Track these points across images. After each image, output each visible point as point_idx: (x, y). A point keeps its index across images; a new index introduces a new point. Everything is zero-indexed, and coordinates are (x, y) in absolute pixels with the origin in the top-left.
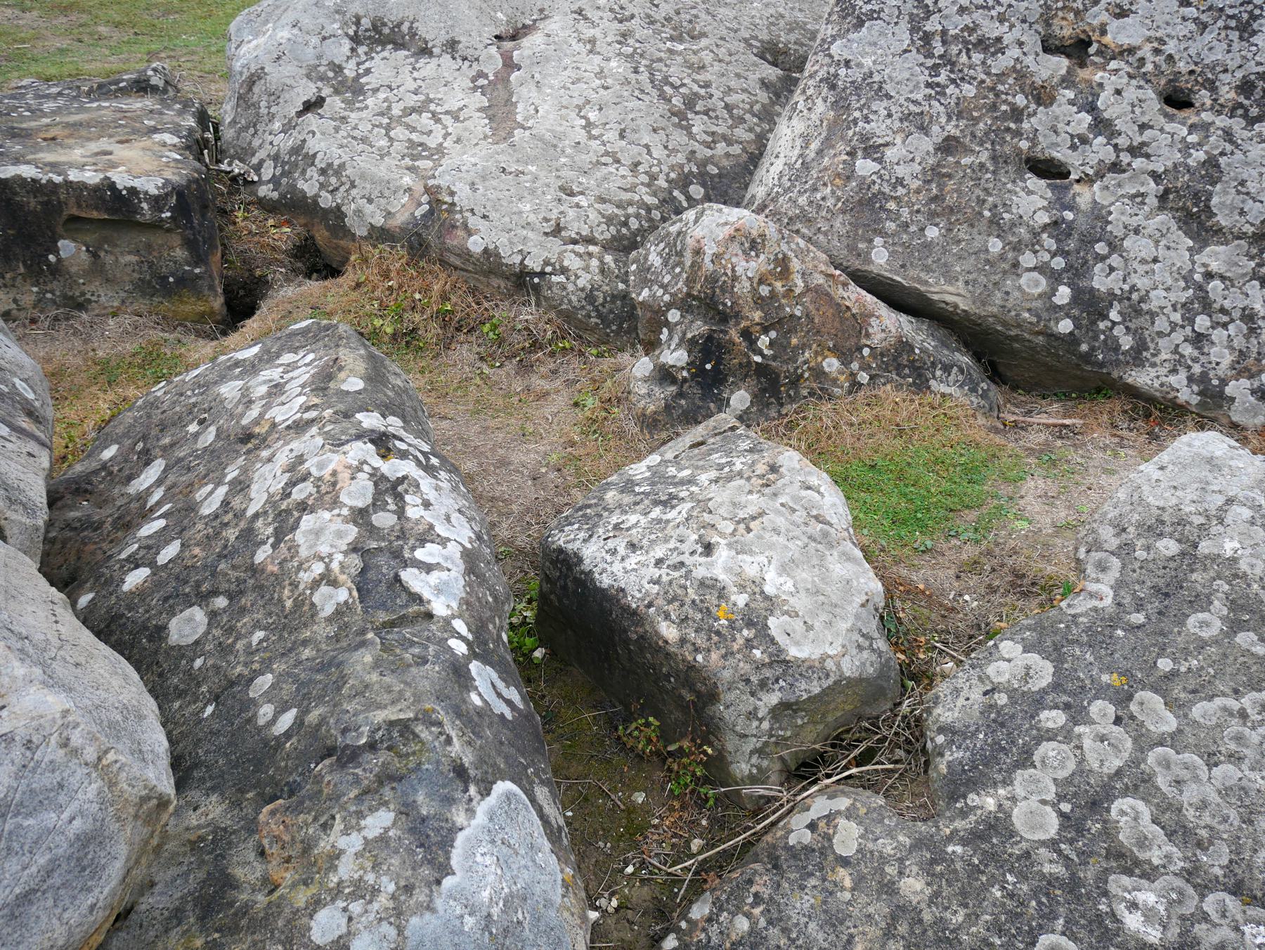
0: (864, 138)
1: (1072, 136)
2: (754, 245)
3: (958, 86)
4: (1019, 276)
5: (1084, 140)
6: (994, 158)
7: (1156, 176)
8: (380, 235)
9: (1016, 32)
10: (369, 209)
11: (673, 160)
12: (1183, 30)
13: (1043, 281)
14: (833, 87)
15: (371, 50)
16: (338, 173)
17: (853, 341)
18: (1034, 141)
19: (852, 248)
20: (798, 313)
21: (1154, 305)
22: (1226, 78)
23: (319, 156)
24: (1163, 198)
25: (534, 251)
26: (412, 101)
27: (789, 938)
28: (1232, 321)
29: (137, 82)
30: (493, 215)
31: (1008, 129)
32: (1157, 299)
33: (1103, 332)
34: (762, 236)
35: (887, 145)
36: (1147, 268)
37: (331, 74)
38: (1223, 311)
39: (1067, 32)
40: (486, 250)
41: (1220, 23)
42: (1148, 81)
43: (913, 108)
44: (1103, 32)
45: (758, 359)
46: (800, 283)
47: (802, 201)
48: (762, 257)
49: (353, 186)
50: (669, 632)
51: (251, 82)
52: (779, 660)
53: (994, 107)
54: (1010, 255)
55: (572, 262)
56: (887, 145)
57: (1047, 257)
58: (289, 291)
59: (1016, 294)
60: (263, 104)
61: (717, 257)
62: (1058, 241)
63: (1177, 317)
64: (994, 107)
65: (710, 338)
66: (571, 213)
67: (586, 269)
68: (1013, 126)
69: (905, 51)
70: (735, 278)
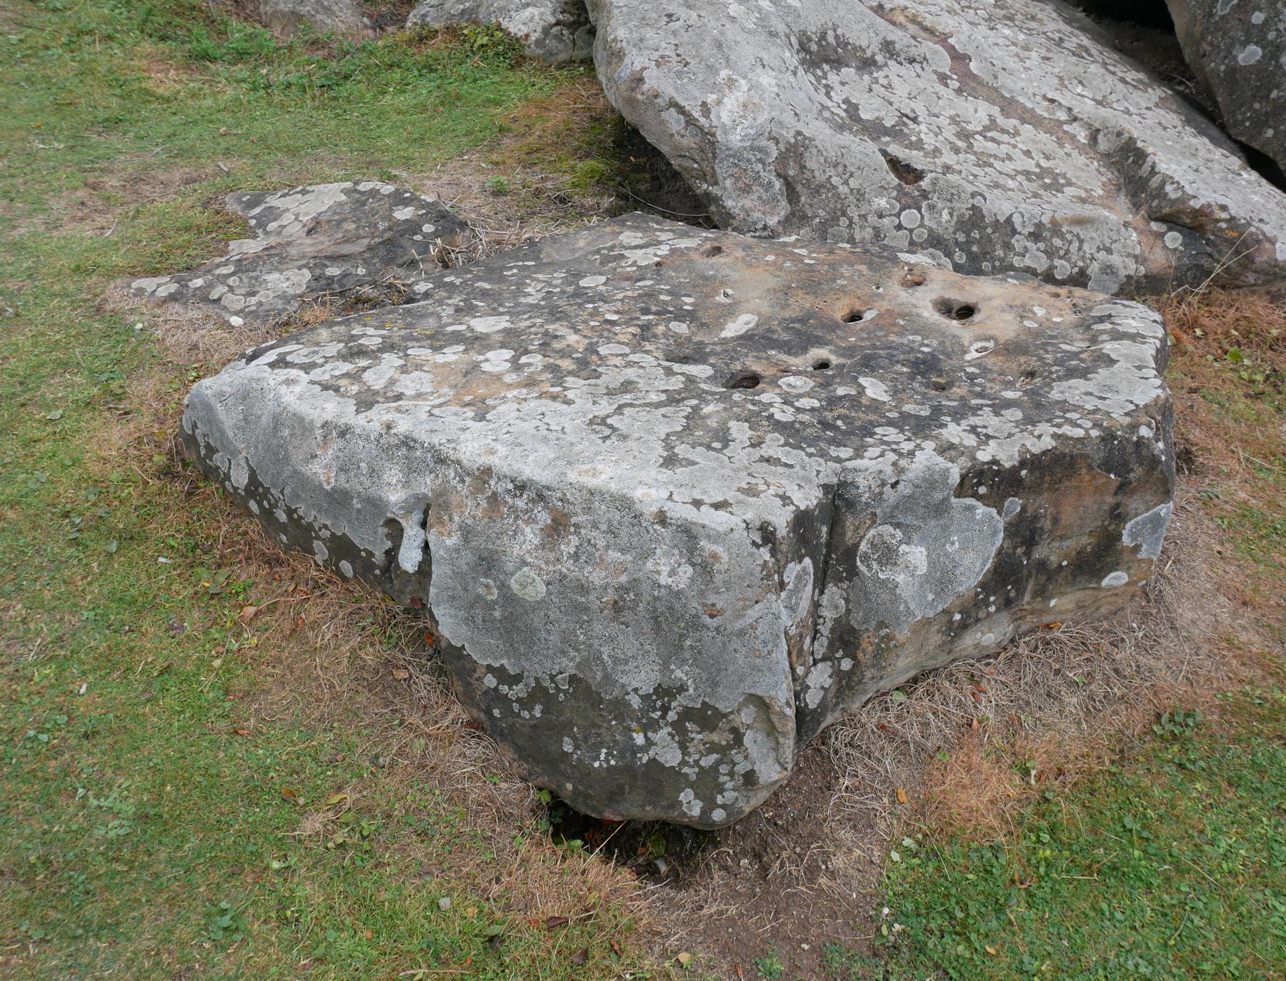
10: (1116, 260)
23: (1017, 219)
60: (835, 180)
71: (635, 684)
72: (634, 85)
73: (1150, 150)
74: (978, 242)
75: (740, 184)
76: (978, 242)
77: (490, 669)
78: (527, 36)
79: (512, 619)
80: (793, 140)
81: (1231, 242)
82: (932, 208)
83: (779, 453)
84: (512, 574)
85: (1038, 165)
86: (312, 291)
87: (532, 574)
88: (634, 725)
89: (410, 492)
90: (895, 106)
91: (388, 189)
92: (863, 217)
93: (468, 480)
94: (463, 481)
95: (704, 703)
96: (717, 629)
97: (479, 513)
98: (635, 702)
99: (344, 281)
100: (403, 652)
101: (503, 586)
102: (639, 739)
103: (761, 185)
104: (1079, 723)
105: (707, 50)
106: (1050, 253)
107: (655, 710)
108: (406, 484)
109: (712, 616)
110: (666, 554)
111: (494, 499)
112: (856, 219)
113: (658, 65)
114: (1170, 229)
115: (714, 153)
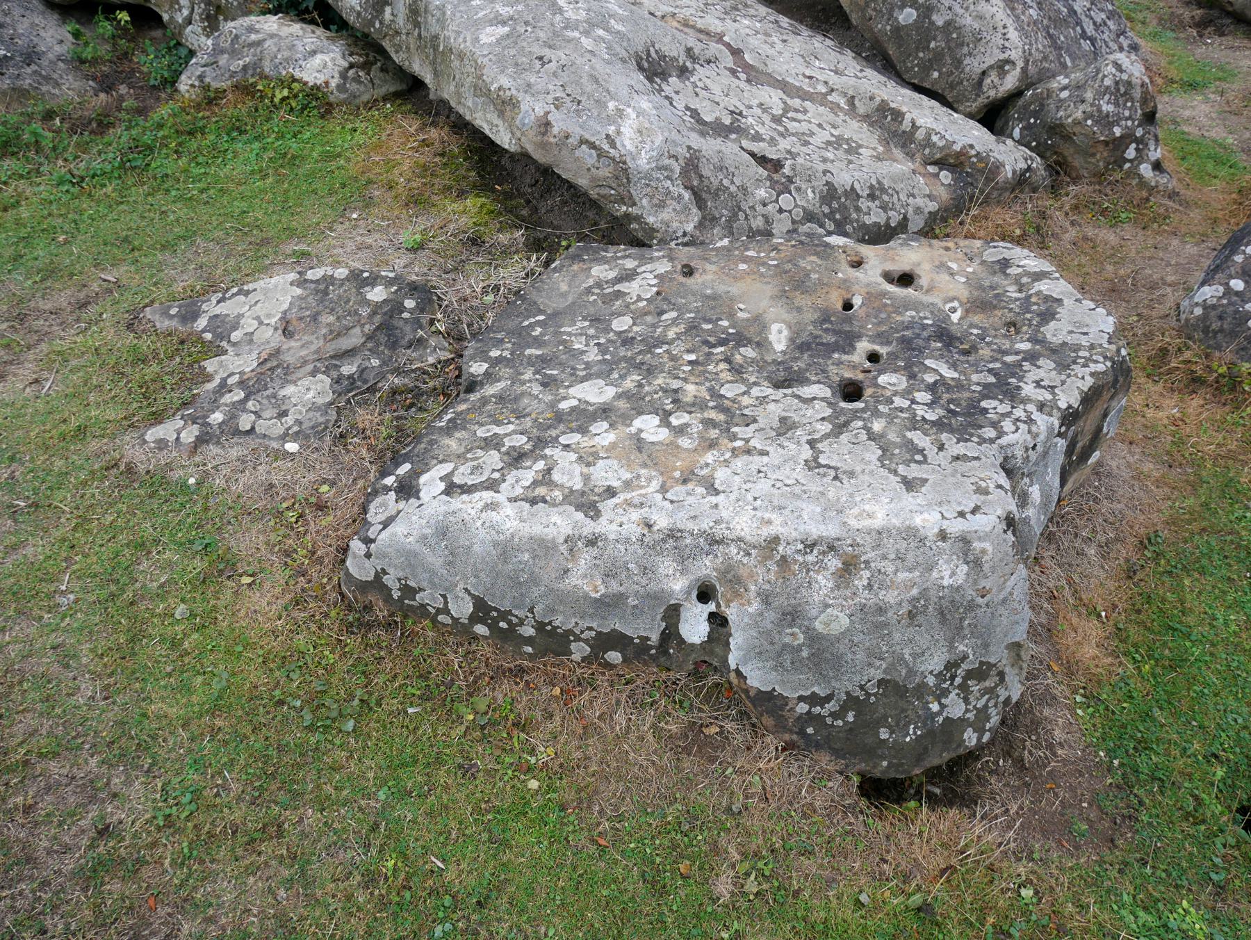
10: (920, 201)
23: (857, 186)
27: (490, 831)
60: (725, 182)
71: (931, 668)
72: (543, 129)
73: (904, 109)
74: (838, 210)
75: (655, 201)
76: (838, 210)
77: (801, 699)
78: (327, 83)
79: (822, 654)
80: (688, 155)
81: (982, 171)
82: (798, 189)
83: (960, 449)
84: (816, 618)
85: (832, 135)
86: (340, 395)
87: (835, 612)
88: (930, 698)
89: (692, 577)
90: (722, 105)
91: (341, 273)
92: (752, 208)
93: (753, 552)
94: (749, 554)
95: (981, 662)
96: (987, 605)
97: (772, 577)
98: (931, 681)
99: (365, 376)
100: (700, 710)
101: (808, 631)
102: (935, 707)
103: (672, 198)
104: (1103, 567)
105: (590, 87)
106: (884, 207)
107: (945, 681)
108: (684, 571)
109: (983, 597)
110: (947, 562)
111: (784, 561)
112: (748, 211)
113: (557, 108)
114: (941, 170)
115: (628, 179)
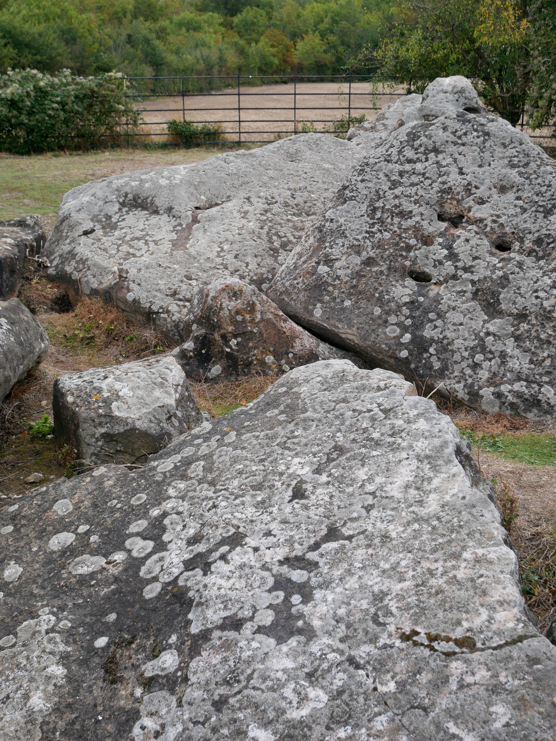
0: (327, 256)
1: (435, 261)
2: (235, 294)
3: (382, 233)
4: (387, 327)
5: (441, 263)
6: (389, 269)
7: (473, 283)
8: (95, 292)
9: (421, 209)
11: (259, 271)
12: (511, 211)
13: (398, 330)
14: (321, 231)
15: (130, 210)
16: (84, 263)
17: (284, 349)
18: (414, 262)
19: (306, 309)
20: (255, 331)
21: (454, 347)
22: (529, 236)
24: (475, 294)
25: (157, 302)
26: (138, 234)
28: (494, 357)
29: (20, 221)
30: (143, 284)
31: (401, 255)
32: (458, 343)
33: (425, 359)
34: (241, 291)
35: (337, 259)
36: (455, 328)
37: (104, 220)
38: (491, 352)
39: (453, 211)
40: (134, 300)
41: (534, 209)
42: (487, 236)
43: (356, 243)
44: (469, 211)
45: (228, 350)
46: (259, 316)
47: (287, 284)
48: (239, 301)
49: (89, 269)
50: (70, 399)
51: (63, 221)
52: (110, 417)
53: (397, 244)
54: (384, 316)
55: (173, 308)
56: (337, 259)
57: (403, 318)
58: (44, 316)
59: (383, 336)
61: (214, 298)
62: (411, 311)
63: (466, 354)
64: (397, 244)
65: (205, 337)
66: (184, 287)
67: (179, 312)
68: (404, 254)
69: (362, 216)
70: (221, 309)
